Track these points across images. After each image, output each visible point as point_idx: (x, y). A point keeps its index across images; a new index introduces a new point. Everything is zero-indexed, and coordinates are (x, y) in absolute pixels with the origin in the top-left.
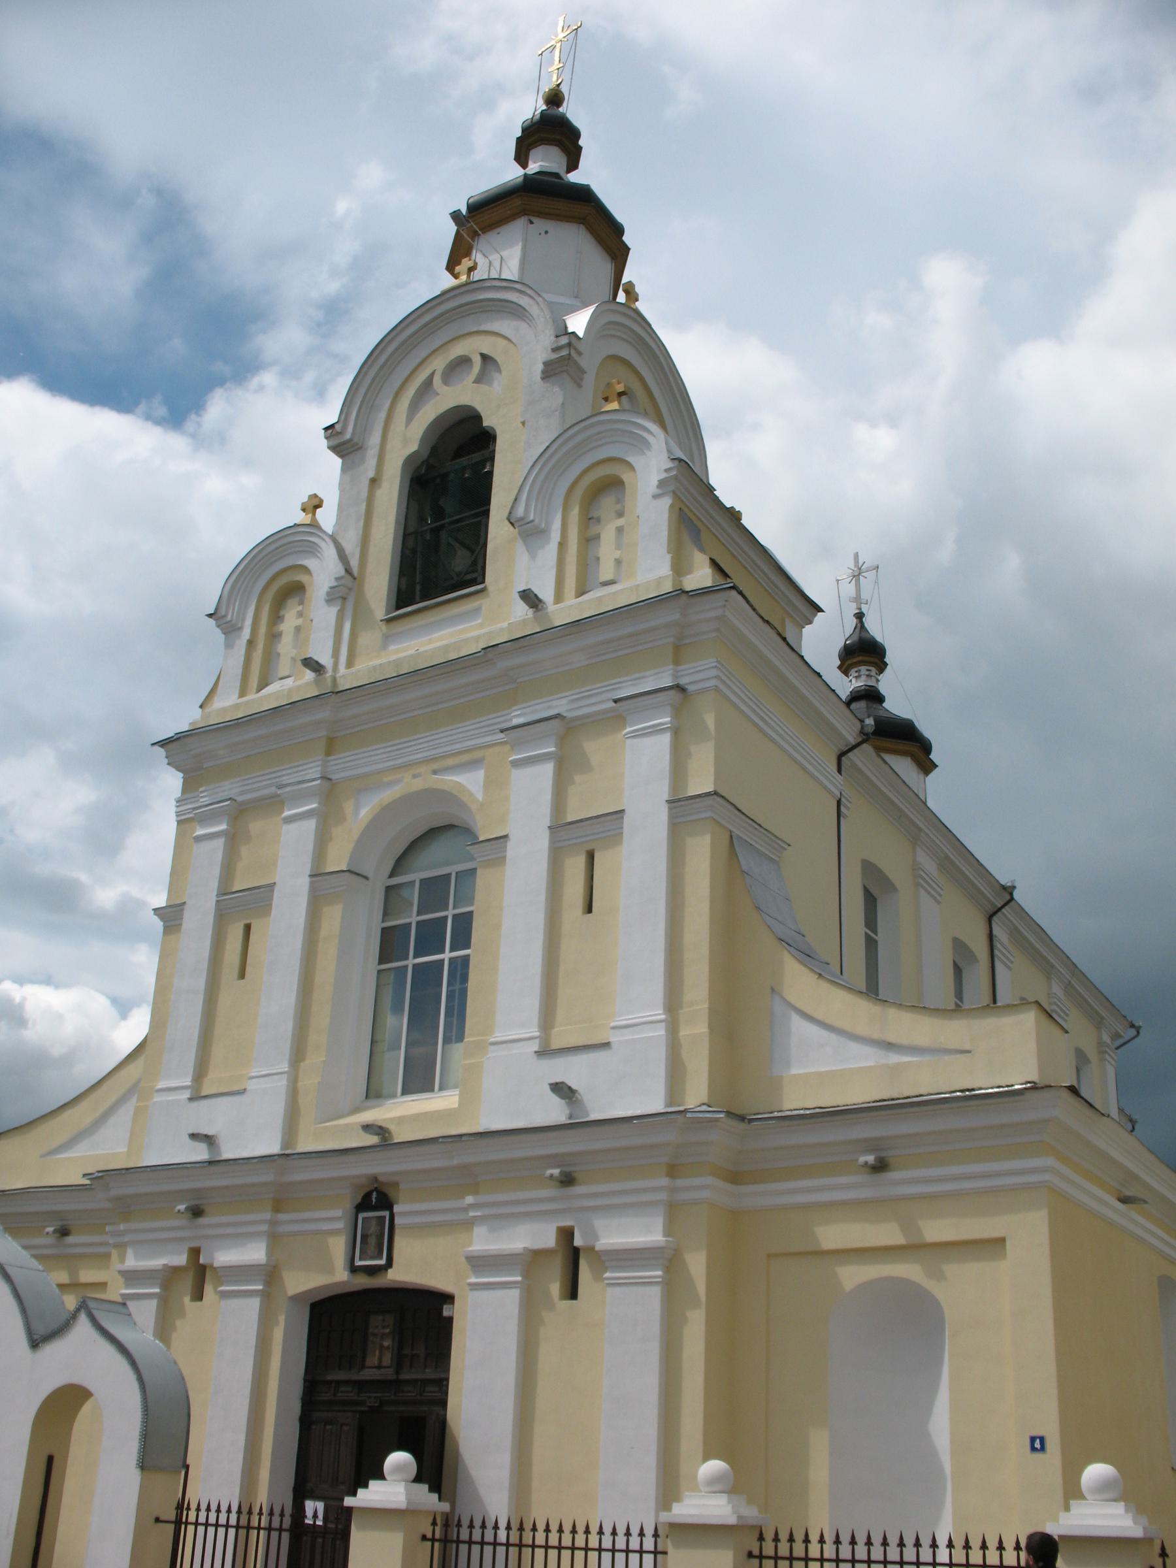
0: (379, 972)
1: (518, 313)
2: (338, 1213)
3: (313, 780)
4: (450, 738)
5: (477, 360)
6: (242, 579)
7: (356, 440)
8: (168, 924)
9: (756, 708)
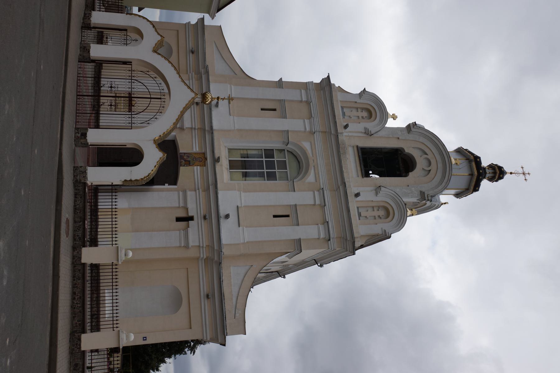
2: (197, 150)
3: (314, 129)
4: (323, 171)
6: (375, 99)
7: (411, 132)
8: (277, 82)
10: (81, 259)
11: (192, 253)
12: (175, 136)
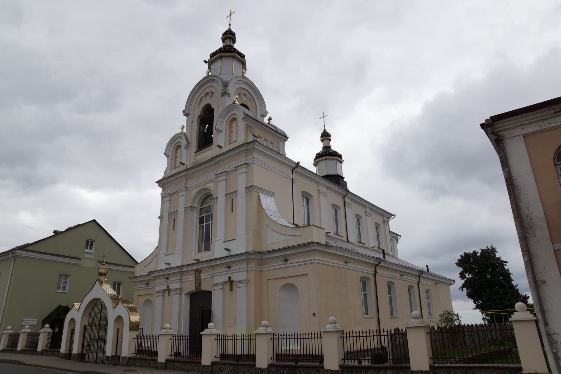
0: (199, 226)
1: (217, 81)
2: (192, 277)
5: (210, 93)
9: (266, 165)
10: (162, 363)
11: (252, 277)
12: (185, 294)
